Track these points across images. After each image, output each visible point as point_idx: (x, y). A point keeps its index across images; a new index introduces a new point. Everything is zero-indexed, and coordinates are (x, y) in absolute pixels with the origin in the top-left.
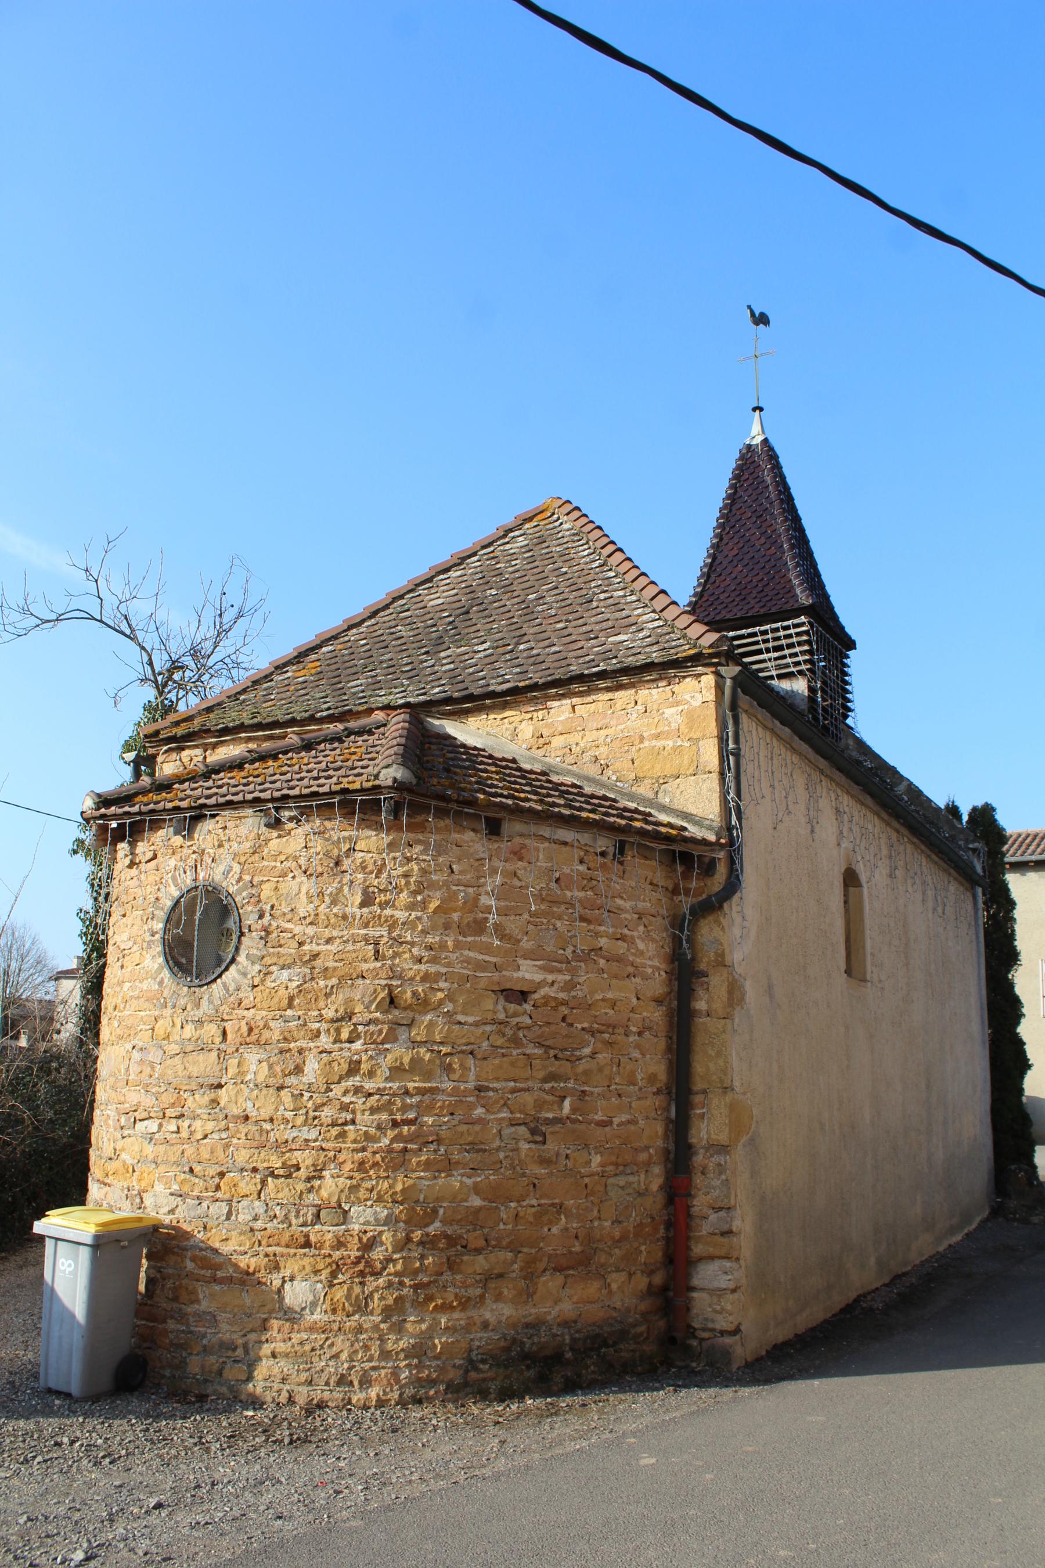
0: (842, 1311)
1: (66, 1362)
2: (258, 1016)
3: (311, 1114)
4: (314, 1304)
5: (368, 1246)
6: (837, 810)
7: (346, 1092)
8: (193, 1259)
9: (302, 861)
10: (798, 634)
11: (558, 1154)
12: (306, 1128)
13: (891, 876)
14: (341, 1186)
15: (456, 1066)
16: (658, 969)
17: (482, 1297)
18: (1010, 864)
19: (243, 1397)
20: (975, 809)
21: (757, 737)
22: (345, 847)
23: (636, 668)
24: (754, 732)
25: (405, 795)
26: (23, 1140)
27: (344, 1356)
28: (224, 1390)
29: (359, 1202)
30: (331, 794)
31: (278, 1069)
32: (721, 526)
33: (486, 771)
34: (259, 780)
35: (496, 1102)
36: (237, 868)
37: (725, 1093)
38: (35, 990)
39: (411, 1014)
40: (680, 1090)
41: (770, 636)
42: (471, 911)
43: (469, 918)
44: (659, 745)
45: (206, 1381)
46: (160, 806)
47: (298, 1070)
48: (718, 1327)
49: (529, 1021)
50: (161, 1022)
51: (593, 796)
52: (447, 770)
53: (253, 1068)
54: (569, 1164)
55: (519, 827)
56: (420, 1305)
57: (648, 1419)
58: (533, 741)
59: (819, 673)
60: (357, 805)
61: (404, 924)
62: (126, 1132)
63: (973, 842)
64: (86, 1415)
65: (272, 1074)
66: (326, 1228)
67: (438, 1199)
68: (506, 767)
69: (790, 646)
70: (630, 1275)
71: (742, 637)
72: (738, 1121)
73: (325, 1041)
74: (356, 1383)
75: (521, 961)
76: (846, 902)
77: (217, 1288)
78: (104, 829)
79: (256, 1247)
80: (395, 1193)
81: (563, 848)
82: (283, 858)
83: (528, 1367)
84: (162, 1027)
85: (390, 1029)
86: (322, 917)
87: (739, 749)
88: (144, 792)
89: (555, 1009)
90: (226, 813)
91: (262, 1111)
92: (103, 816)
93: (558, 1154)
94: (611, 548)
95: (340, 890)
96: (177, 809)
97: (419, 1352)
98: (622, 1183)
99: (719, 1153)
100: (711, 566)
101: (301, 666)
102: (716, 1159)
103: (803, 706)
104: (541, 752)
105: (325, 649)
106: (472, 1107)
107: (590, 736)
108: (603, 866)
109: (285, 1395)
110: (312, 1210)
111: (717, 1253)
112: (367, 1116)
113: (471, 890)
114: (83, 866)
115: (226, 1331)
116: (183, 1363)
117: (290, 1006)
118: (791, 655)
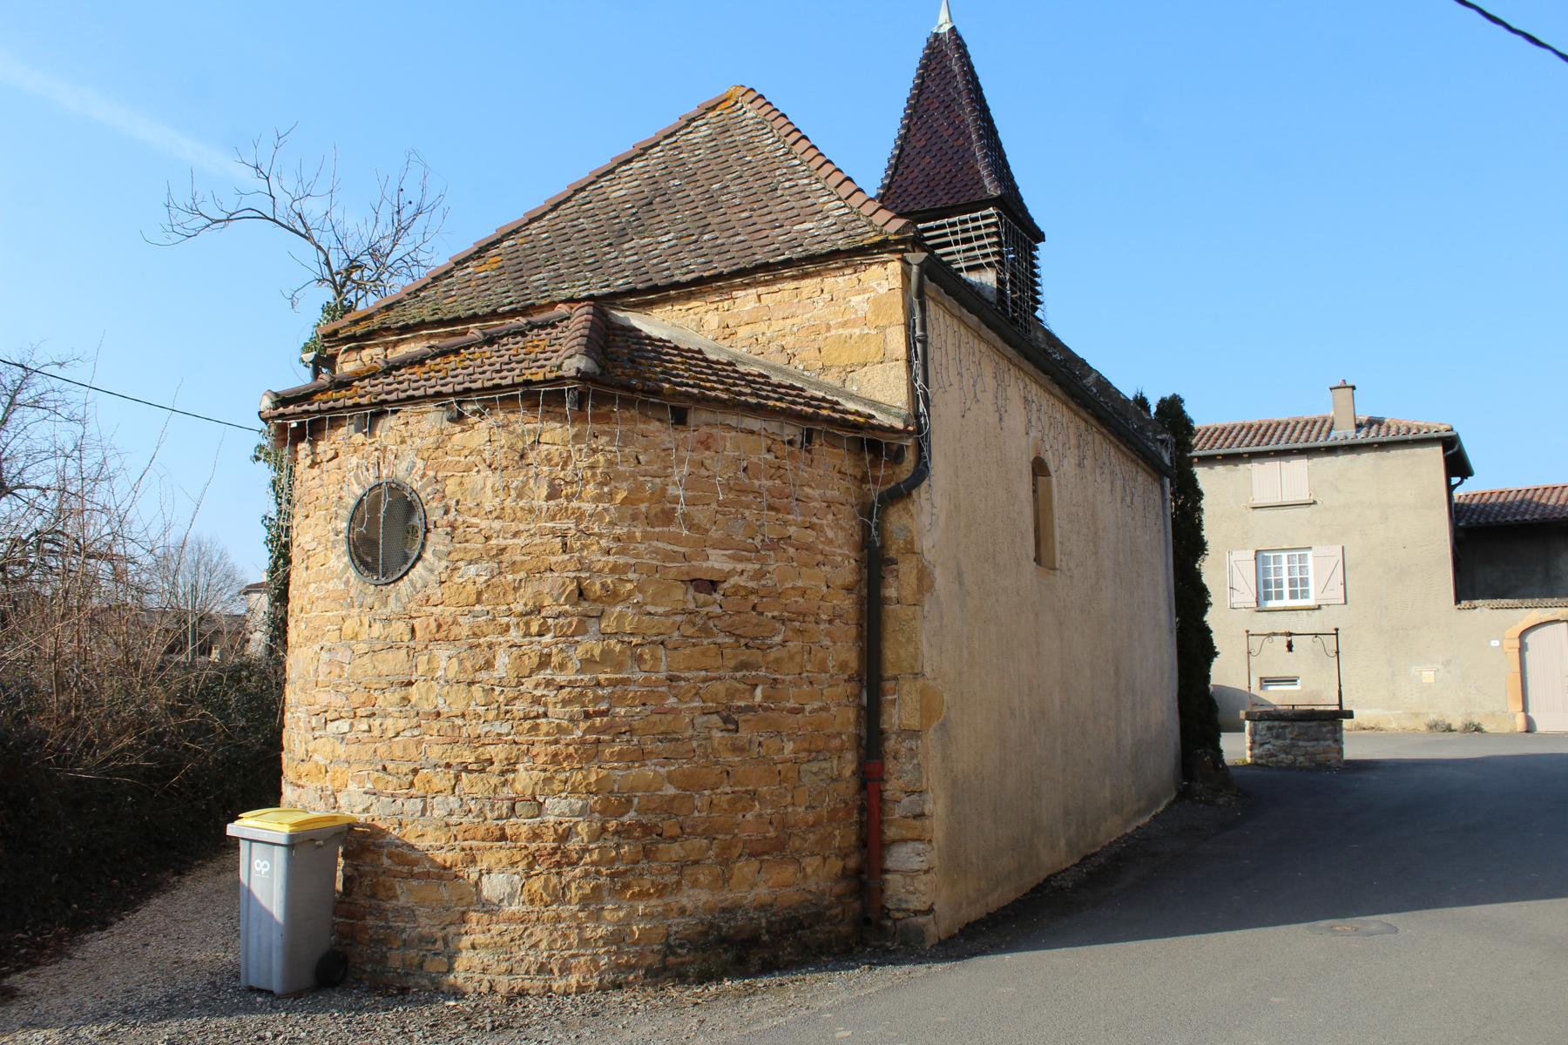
0: (1033, 890)
1: (265, 958)
2: (446, 612)
3: (503, 708)
4: (512, 896)
5: (564, 837)
6: (1026, 400)
7: (537, 686)
8: (390, 856)
9: (486, 455)
10: (986, 226)
13: (1080, 465)
15: (647, 657)
17: (679, 883)
18: (1199, 458)
19: (445, 988)
20: (1163, 401)
21: (943, 325)
22: (529, 440)
23: (822, 255)
26: (215, 748)
27: (543, 945)
28: (425, 982)
29: (554, 794)
30: (514, 386)
31: (468, 664)
32: (909, 117)
33: (671, 362)
34: (441, 375)
36: (420, 464)
38: (224, 605)
39: (600, 606)
40: (871, 677)
41: (958, 228)
43: (657, 508)
44: (846, 333)
45: (407, 974)
46: (340, 404)
47: (489, 665)
48: (911, 907)
50: (348, 622)
51: (780, 386)
52: (633, 362)
53: (443, 664)
55: (705, 416)
56: (614, 893)
57: (844, 995)
58: (719, 331)
59: (1008, 265)
60: (541, 397)
61: (591, 516)
62: (317, 734)
64: (288, 1011)
66: (521, 821)
67: (632, 789)
68: (692, 358)
70: (825, 859)
72: (929, 707)
73: (514, 635)
74: (556, 971)
75: (710, 551)
76: (1035, 491)
77: (415, 883)
78: (282, 429)
80: (589, 784)
83: (726, 951)
84: (349, 627)
85: (580, 621)
86: (508, 511)
88: (324, 390)
89: (745, 597)
90: (408, 408)
91: (454, 707)
92: (281, 416)
93: (750, 742)
94: (796, 136)
95: (525, 483)
97: (617, 939)
98: (815, 769)
100: (899, 157)
101: (481, 261)
102: (908, 744)
103: (993, 298)
104: (727, 343)
105: (506, 244)
106: (663, 697)
107: (777, 325)
109: (486, 985)
110: (507, 804)
111: (910, 835)
113: (658, 480)
114: (265, 472)
115: (426, 925)
116: (384, 958)
117: (479, 601)
118: (980, 247)
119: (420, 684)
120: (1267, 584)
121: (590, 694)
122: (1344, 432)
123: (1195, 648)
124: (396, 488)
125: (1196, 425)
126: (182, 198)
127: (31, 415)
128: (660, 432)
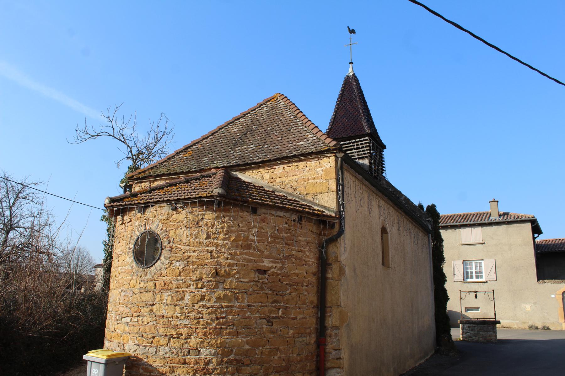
3: (187, 315)
5: (207, 363)
6: (379, 206)
7: (200, 307)
8: (143, 369)
9: (185, 222)
10: (365, 143)
15: (240, 297)
16: (314, 262)
20: (429, 206)
29: (204, 347)
30: (196, 198)
31: (175, 298)
35: (255, 310)
36: (161, 225)
39: (224, 278)
40: (322, 307)
42: (246, 241)
43: (245, 243)
44: (315, 182)
46: (133, 202)
47: (182, 299)
50: (132, 281)
51: (291, 200)
52: (238, 190)
53: (166, 298)
54: (281, 333)
55: (264, 210)
59: (373, 157)
60: (205, 202)
62: (118, 322)
63: (428, 218)
65: (173, 300)
66: (192, 357)
67: (233, 346)
72: (343, 317)
73: (192, 288)
75: (264, 259)
78: (112, 211)
79: (166, 364)
80: (217, 344)
82: (177, 221)
84: (133, 283)
87: (343, 183)
89: (276, 276)
90: (157, 205)
92: (112, 206)
93: (277, 330)
94: (298, 111)
95: (198, 233)
96: (139, 203)
98: (300, 340)
99: (336, 329)
100: (334, 119)
102: (335, 332)
104: (272, 184)
106: (246, 312)
107: (290, 178)
108: (294, 225)
110: (187, 350)
112: (207, 315)
113: (246, 233)
117: (180, 275)
118: (363, 151)
119: (157, 305)
120: (467, 273)
122: (495, 217)
123: (441, 296)
125: (441, 215)
126: (82, 128)
127: (24, 201)
128: (247, 216)
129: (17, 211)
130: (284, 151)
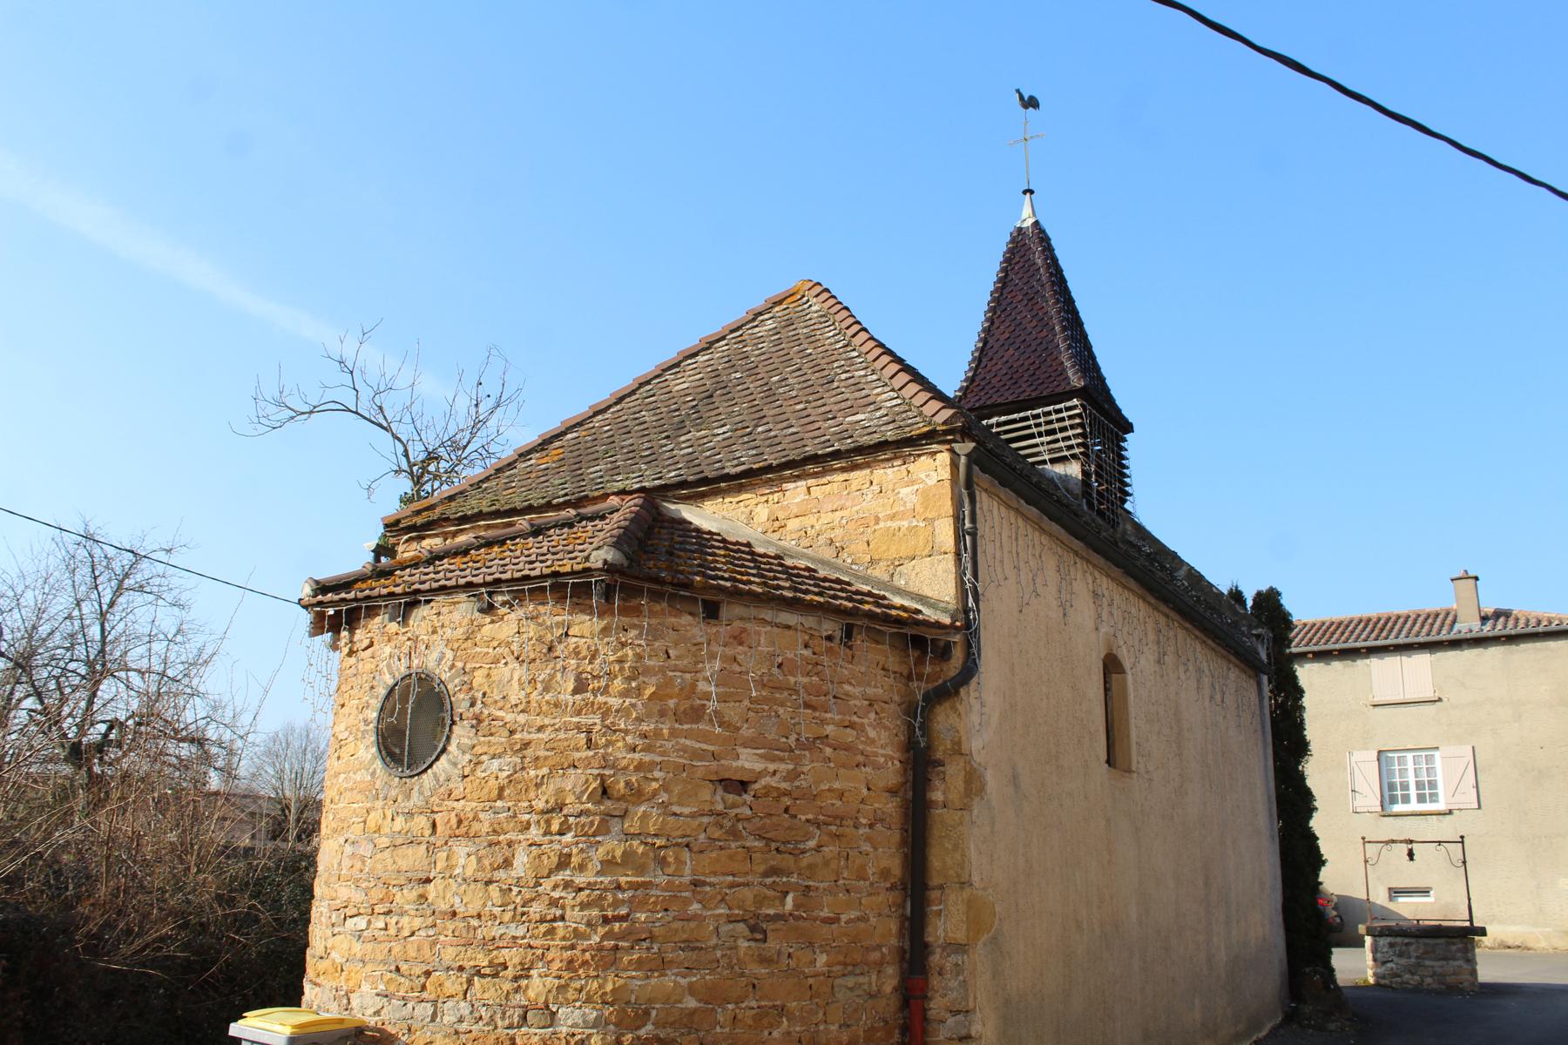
2: (468, 807)
3: (520, 909)
6: (1095, 594)
7: (555, 887)
10: (1070, 417)
11: (779, 953)
12: (513, 925)
14: (549, 986)
15: (671, 860)
16: (892, 758)
20: (1259, 594)
24: (995, 512)
25: (617, 577)
29: (568, 1003)
30: (543, 577)
31: (486, 862)
32: (992, 310)
36: (449, 655)
37: (962, 888)
39: (624, 805)
40: (916, 886)
43: (686, 704)
44: (894, 527)
47: (507, 863)
49: (749, 812)
50: (373, 814)
51: (825, 580)
52: (671, 554)
53: (462, 861)
55: (738, 610)
58: (768, 524)
59: (1093, 456)
60: (569, 588)
61: (617, 711)
62: (336, 930)
63: (1257, 627)
65: (481, 868)
66: (533, 1030)
67: (650, 1001)
69: (1063, 429)
71: (1014, 421)
72: (978, 918)
73: (535, 833)
75: (740, 750)
80: (605, 994)
81: (787, 632)
82: (495, 643)
84: (374, 818)
85: (602, 821)
86: (534, 704)
89: (777, 799)
92: (320, 603)
93: (779, 953)
94: (856, 328)
95: (552, 676)
96: (391, 594)
98: (850, 984)
100: (982, 350)
102: (953, 959)
104: (776, 536)
107: (826, 518)
108: (829, 651)
110: (519, 1012)
113: (688, 676)
117: (500, 797)
118: (1064, 439)
119: (438, 881)
120: (1392, 787)
121: (610, 898)
122: (1468, 625)
123: (1300, 856)
124: (425, 679)
126: (271, 391)
127: (138, 598)
128: (691, 625)
129: (117, 626)
130: (809, 442)
